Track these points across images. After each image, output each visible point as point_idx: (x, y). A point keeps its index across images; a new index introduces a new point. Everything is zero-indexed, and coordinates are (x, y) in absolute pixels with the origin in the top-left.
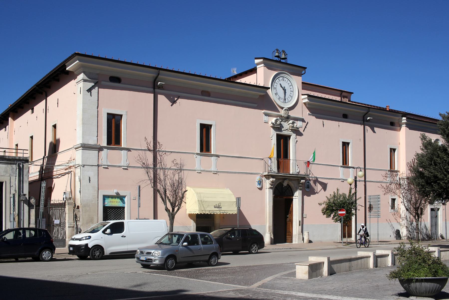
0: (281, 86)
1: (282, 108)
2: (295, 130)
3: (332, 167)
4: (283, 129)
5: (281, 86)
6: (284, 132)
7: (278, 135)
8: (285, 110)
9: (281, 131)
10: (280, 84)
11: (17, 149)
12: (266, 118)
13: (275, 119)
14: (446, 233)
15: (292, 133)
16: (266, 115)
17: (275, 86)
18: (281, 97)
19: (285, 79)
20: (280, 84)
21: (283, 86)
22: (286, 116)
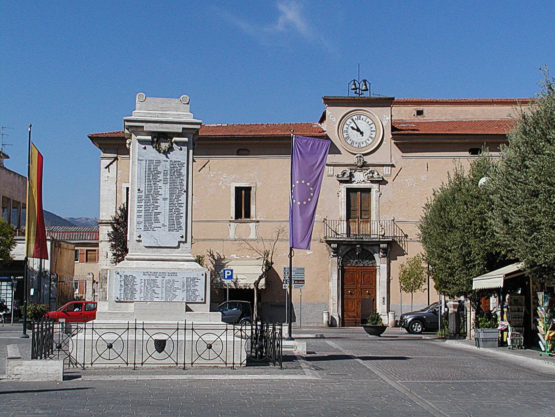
15: (371, 184)
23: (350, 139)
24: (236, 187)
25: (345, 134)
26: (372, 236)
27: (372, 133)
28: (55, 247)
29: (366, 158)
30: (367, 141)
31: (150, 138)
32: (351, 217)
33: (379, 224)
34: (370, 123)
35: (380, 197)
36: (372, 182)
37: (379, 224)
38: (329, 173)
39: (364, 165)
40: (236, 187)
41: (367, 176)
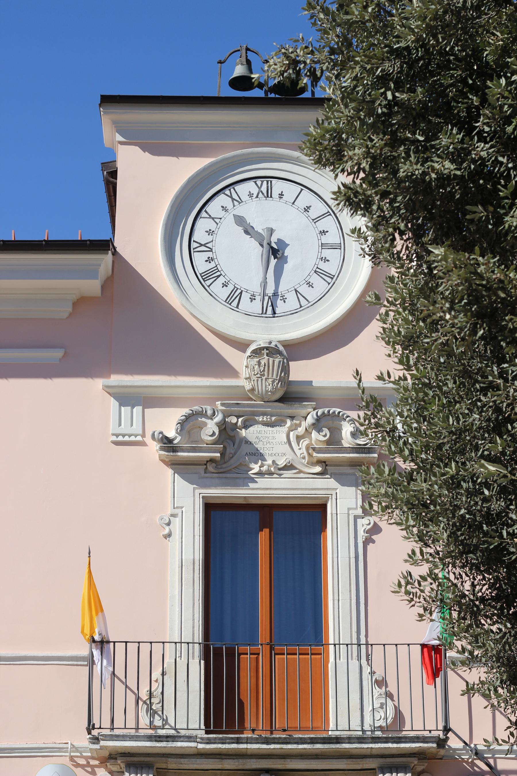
0: (249, 231)
1: (241, 345)
2: (355, 464)
3: (347, 713)
4: (256, 468)
5: (249, 231)
6: (263, 482)
7: (210, 508)
8: (257, 352)
9: (242, 477)
10: (240, 220)
11: (339, 644)
12: (131, 420)
13: (179, 413)
14: (238, 195)
15: (330, 482)
16: (126, 398)
17: (200, 236)
18: (243, 285)
19: (278, 186)
20: (240, 220)
21: (259, 228)
22: (267, 386)
23: (221, 280)
24: (101, 96)
25: (200, 259)
26: (330, 733)
27: (326, 253)
28: (345, 205)
29: (300, 371)
30: (304, 289)
31: (438, 655)
32: (383, 717)
33: (366, 670)
34: (314, 213)
35: (368, 541)
36: (327, 468)
37: (366, 670)
38: (124, 428)
39: (291, 396)
40: (101, 96)
41: (305, 443)
